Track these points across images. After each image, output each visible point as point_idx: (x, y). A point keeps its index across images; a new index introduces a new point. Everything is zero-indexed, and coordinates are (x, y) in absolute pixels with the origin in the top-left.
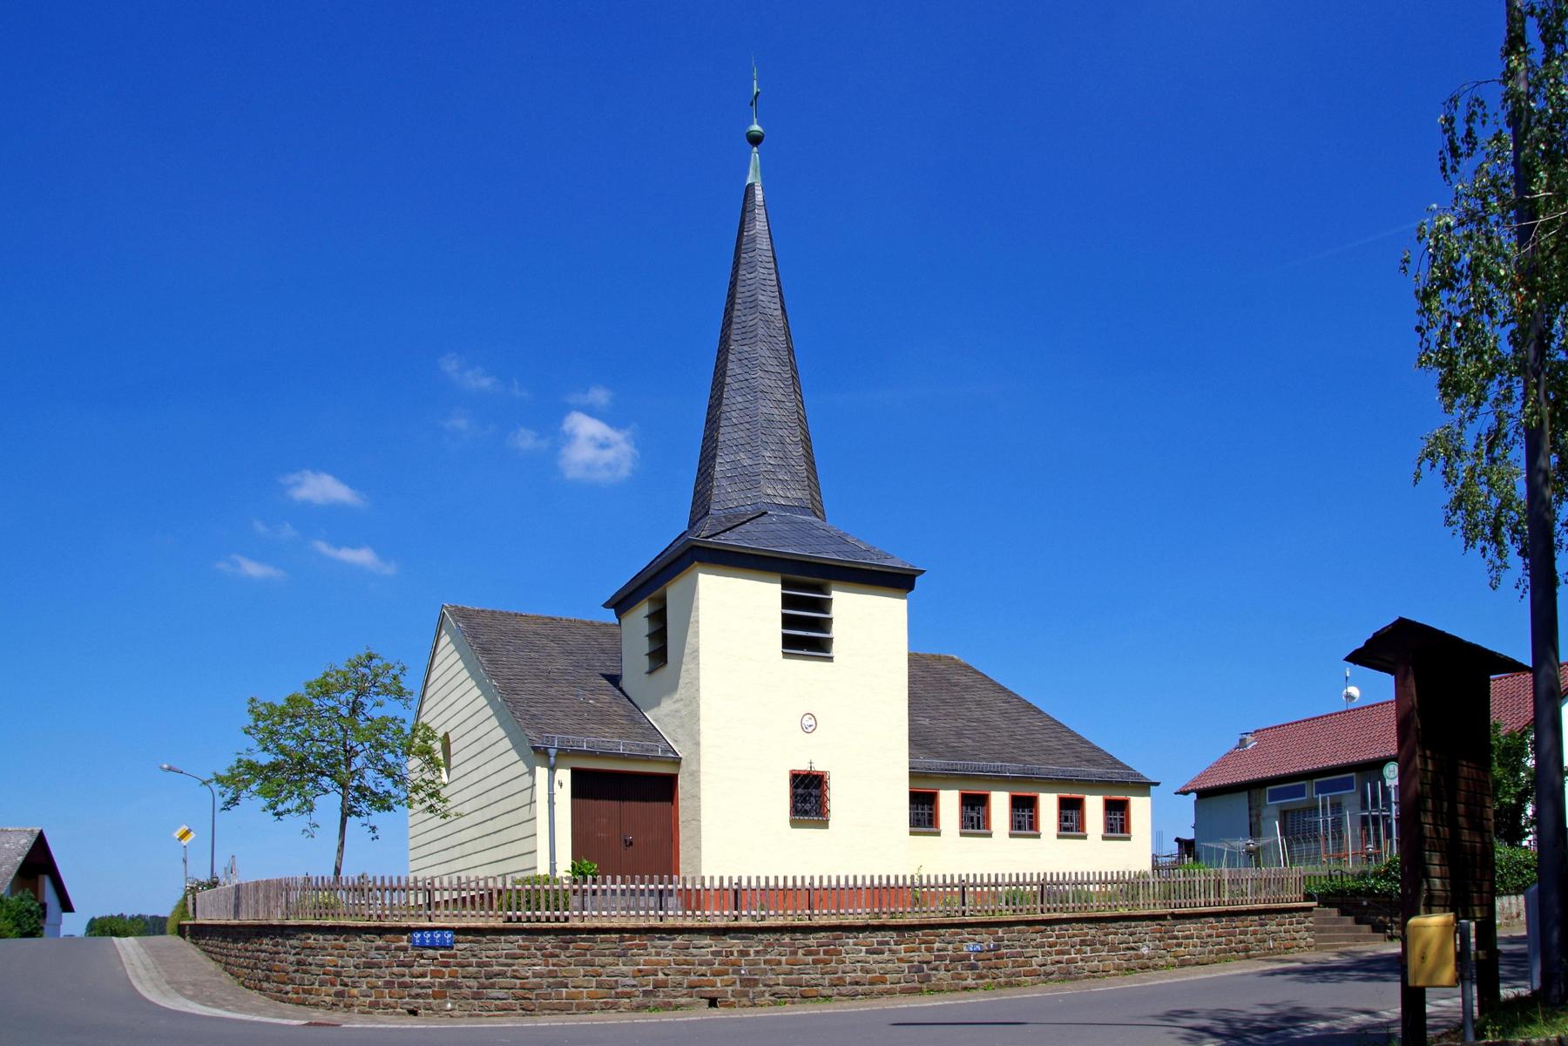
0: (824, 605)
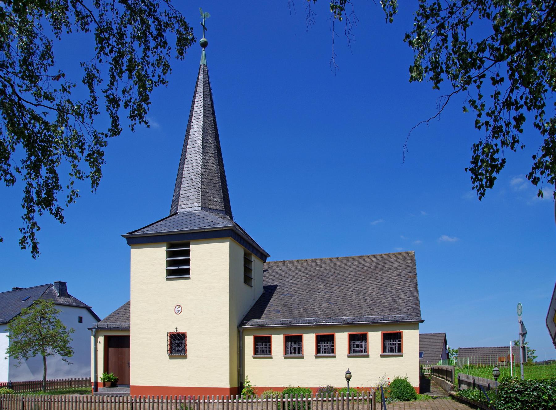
0: (188, 253)
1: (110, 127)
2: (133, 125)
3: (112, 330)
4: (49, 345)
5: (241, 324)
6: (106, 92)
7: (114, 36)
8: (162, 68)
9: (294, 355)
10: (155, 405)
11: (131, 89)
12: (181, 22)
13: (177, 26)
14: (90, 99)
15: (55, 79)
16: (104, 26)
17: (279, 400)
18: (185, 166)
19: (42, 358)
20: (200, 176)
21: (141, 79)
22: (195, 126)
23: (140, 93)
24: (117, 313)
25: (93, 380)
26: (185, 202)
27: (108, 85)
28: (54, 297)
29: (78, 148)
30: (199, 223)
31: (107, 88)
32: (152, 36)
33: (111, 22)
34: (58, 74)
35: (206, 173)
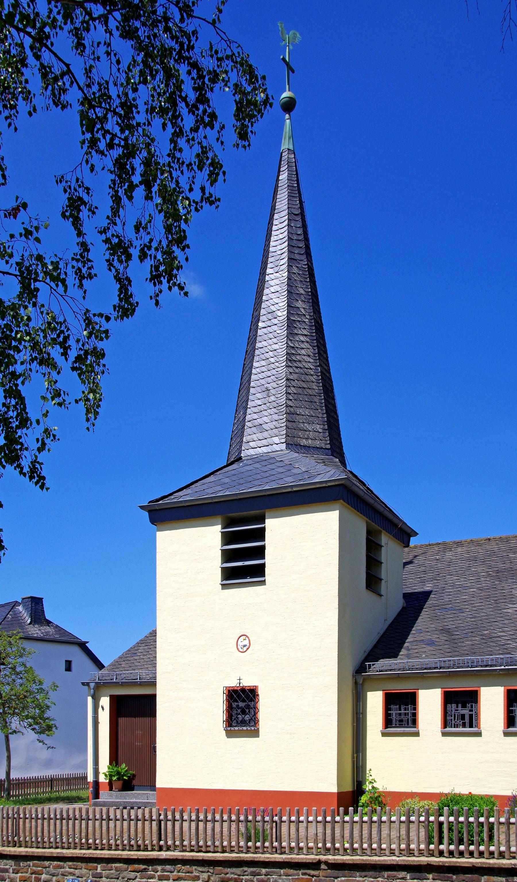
0: (260, 534)
1: (116, 301)
2: (157, 295)
3: (123, 684)
4: (14, 714)
5: (361, 669)
6: (103, 231)
7: (115, 113)
8: (206, 171)
9: (461, 729)
10: (201, 824)
11: (150, 222)
12: (242, 65)
13: (234, 77)
14: (77, 250)
15: (10, 214)
16: (94, 93)
17: (432, 819)
18: (255, 364)
19: (4, 738)
20: (283, 382)
21: (169, 197)
22: (272, 283)
23: (168, 229)
24: (132, 652)
25: (90, 778)
26: (254, 437)
27: (108, 217)
28: (22, 625)
29: (58, 346)
30: (282, 476)
31: (105, 223)
32: (187, 105)
33: (107, 83)
34: (14, 204)
35: (295, 376)
